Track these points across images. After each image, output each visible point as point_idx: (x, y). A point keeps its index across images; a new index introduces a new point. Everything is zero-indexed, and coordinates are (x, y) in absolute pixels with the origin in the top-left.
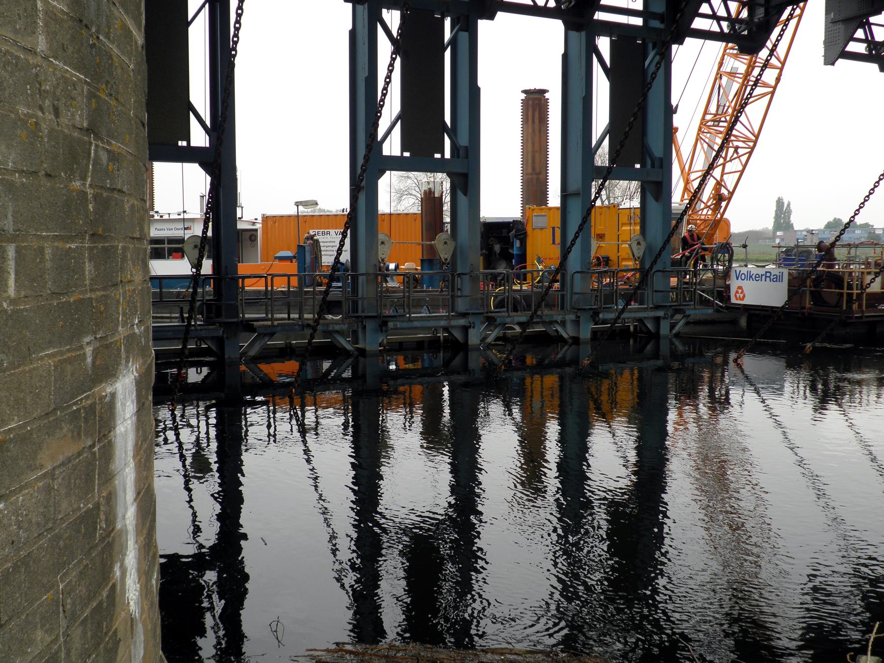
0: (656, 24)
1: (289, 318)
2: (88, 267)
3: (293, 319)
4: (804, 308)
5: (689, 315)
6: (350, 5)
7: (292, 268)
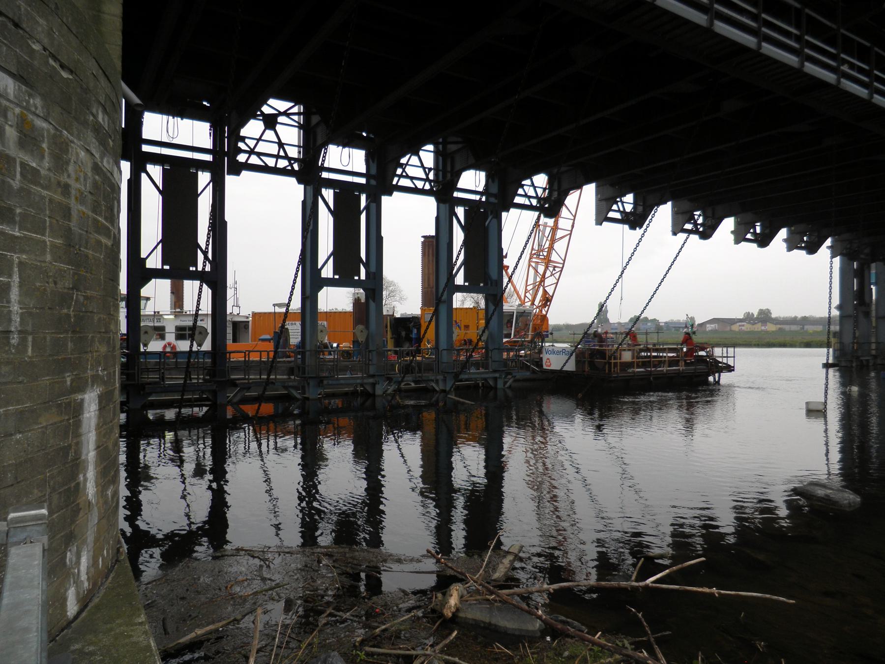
0: (493, 200)
1: (260, 378)
2: (70, 344)
3: (263, 379)
4: (585, 371)
5: (515, 376)
6: (302, 186)
7: (271, 346)
